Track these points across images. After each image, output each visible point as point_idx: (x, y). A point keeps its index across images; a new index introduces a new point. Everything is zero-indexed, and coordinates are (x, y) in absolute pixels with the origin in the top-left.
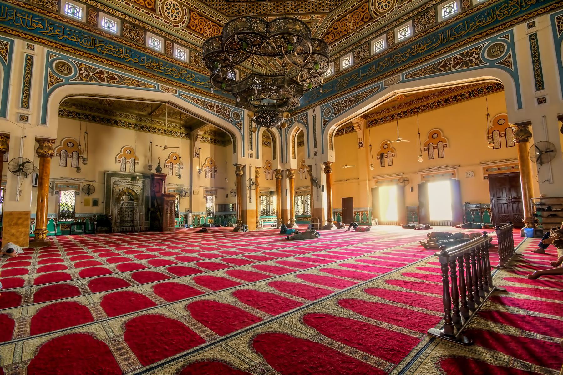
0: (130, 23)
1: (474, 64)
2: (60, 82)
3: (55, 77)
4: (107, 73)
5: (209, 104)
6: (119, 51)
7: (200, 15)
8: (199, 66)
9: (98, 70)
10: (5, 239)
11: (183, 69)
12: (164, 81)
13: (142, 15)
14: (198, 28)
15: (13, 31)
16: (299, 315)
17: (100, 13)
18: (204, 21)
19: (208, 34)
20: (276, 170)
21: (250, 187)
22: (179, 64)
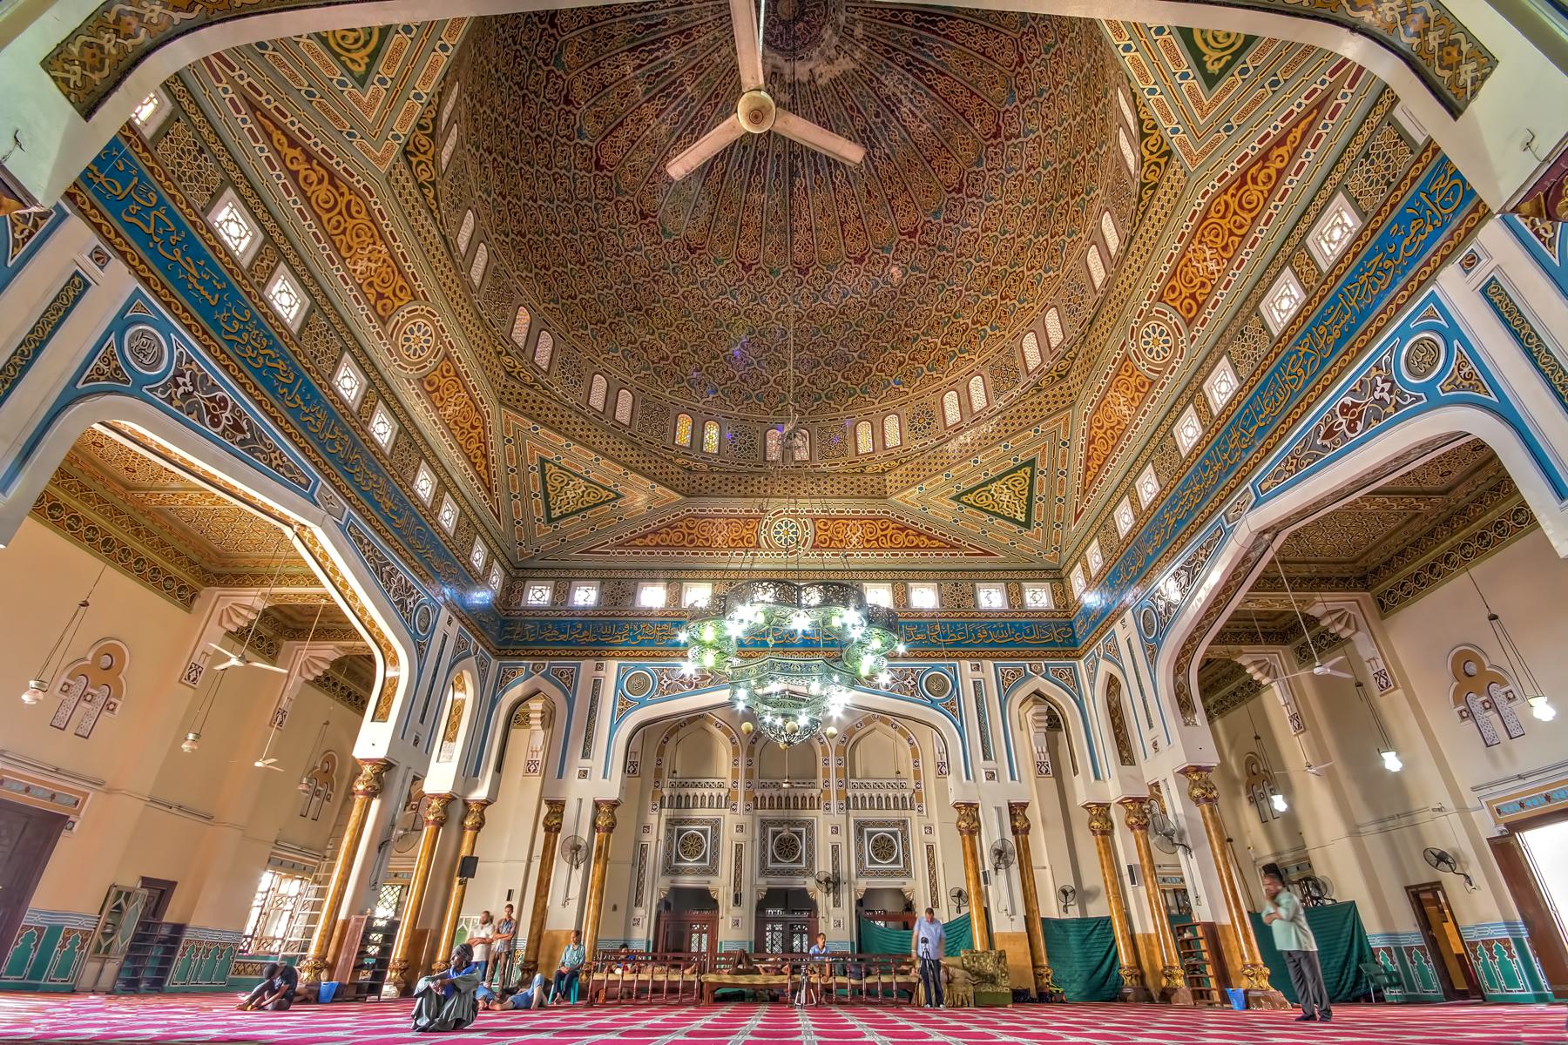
2: (118, 381)
3: (113, 364)
7: (457, 375)
9: (220, 394)
13: (358, 315)
14: (342, 237)
16: (1225, 920)
18: (372, 236)
19: (448, 412)
22: (364, 440)
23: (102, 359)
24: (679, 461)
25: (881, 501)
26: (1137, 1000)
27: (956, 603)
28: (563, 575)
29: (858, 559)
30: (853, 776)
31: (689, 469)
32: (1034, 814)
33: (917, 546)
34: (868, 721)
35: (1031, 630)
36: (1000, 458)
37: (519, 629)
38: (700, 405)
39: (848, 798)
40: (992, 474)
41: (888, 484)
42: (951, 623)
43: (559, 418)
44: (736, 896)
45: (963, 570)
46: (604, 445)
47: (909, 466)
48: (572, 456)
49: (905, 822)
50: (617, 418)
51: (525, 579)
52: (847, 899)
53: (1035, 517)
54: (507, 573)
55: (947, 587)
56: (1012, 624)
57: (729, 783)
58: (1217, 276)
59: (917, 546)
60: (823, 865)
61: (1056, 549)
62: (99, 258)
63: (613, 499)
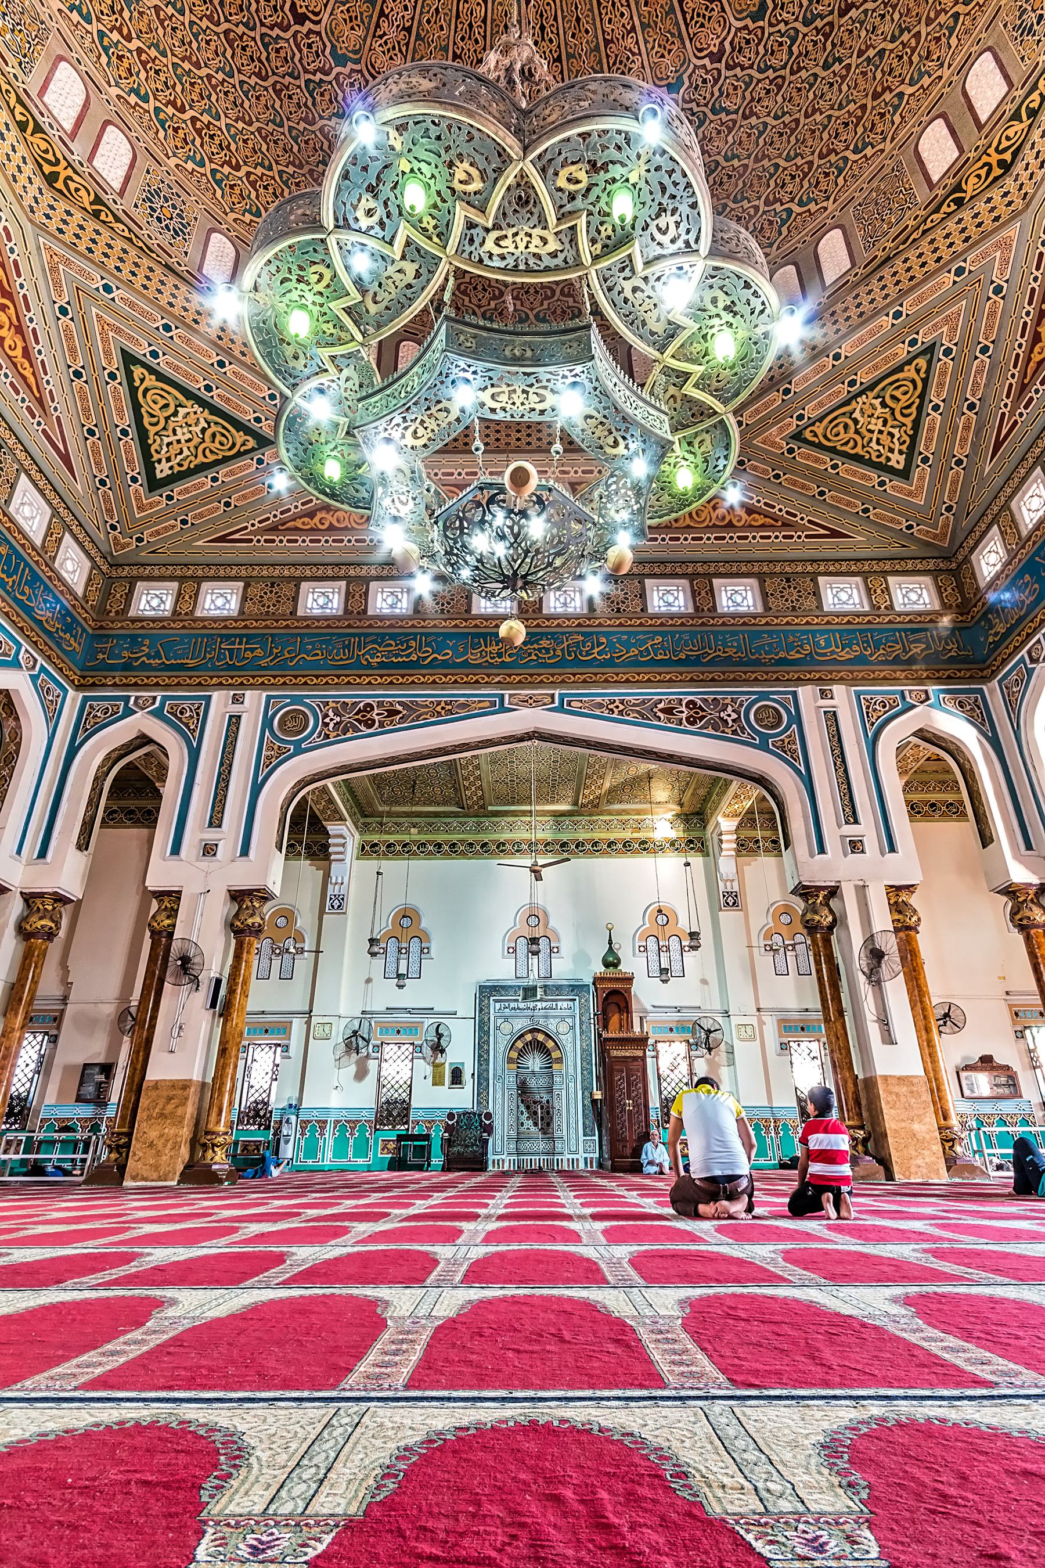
4: (380, 704)
5: (660, 706)
6: (409, 647)
8: (618, 610)
10: (135, 1154)
11: (571, 633)
12: (520, 682)
15: (211, 678)
17: (716, 582)
20: (1010, 891)
21: (874, 977)
23: (267, 750)
26: (603, 1044)
62: (237, 700)
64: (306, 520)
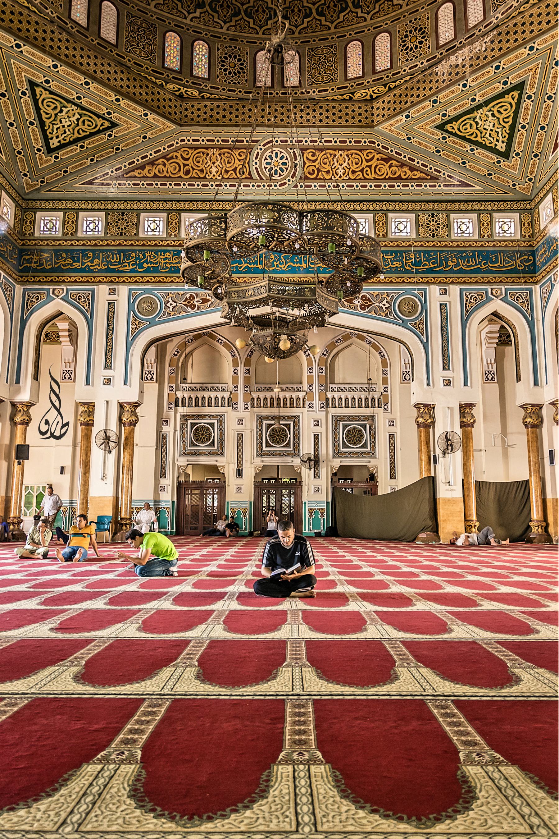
0: (321, 211)
1: (383, 314)
3: (137, 323)
14: (195, 171)
24: (170, 86)
25: (368, 130)
27: (431, 233)
28: (70, 206)
29: (347, 192)
30: (332, 382)
31: (181, 96)
32: (478, 412)
33: (399, 178)
34: (346, 337)
35: (496, 258)
36: (490, 82)
37: (35, 258)
38: (188, 21)
39: (327, 399)
40: (480, 99)
41: (375, 112)
42: (425, 252)
43: (40, 34)
44: (239, 470)
45: (440, 202)
46: (92, 68)
47: (397, 92)
48: (60, 79)
49: (373, 417)
50: (73, 17)
51: (35, 210)
52: (325, 472)
53: (515, 147)
54: (17, 205)
55: (424, 218)
56: (480, 253)
57: (231, 386)
58: (337, 177)
59: (399, 178)
60: (307, 448)
61: (530, 180)
63: (108, 128)
64: (139, 171)
